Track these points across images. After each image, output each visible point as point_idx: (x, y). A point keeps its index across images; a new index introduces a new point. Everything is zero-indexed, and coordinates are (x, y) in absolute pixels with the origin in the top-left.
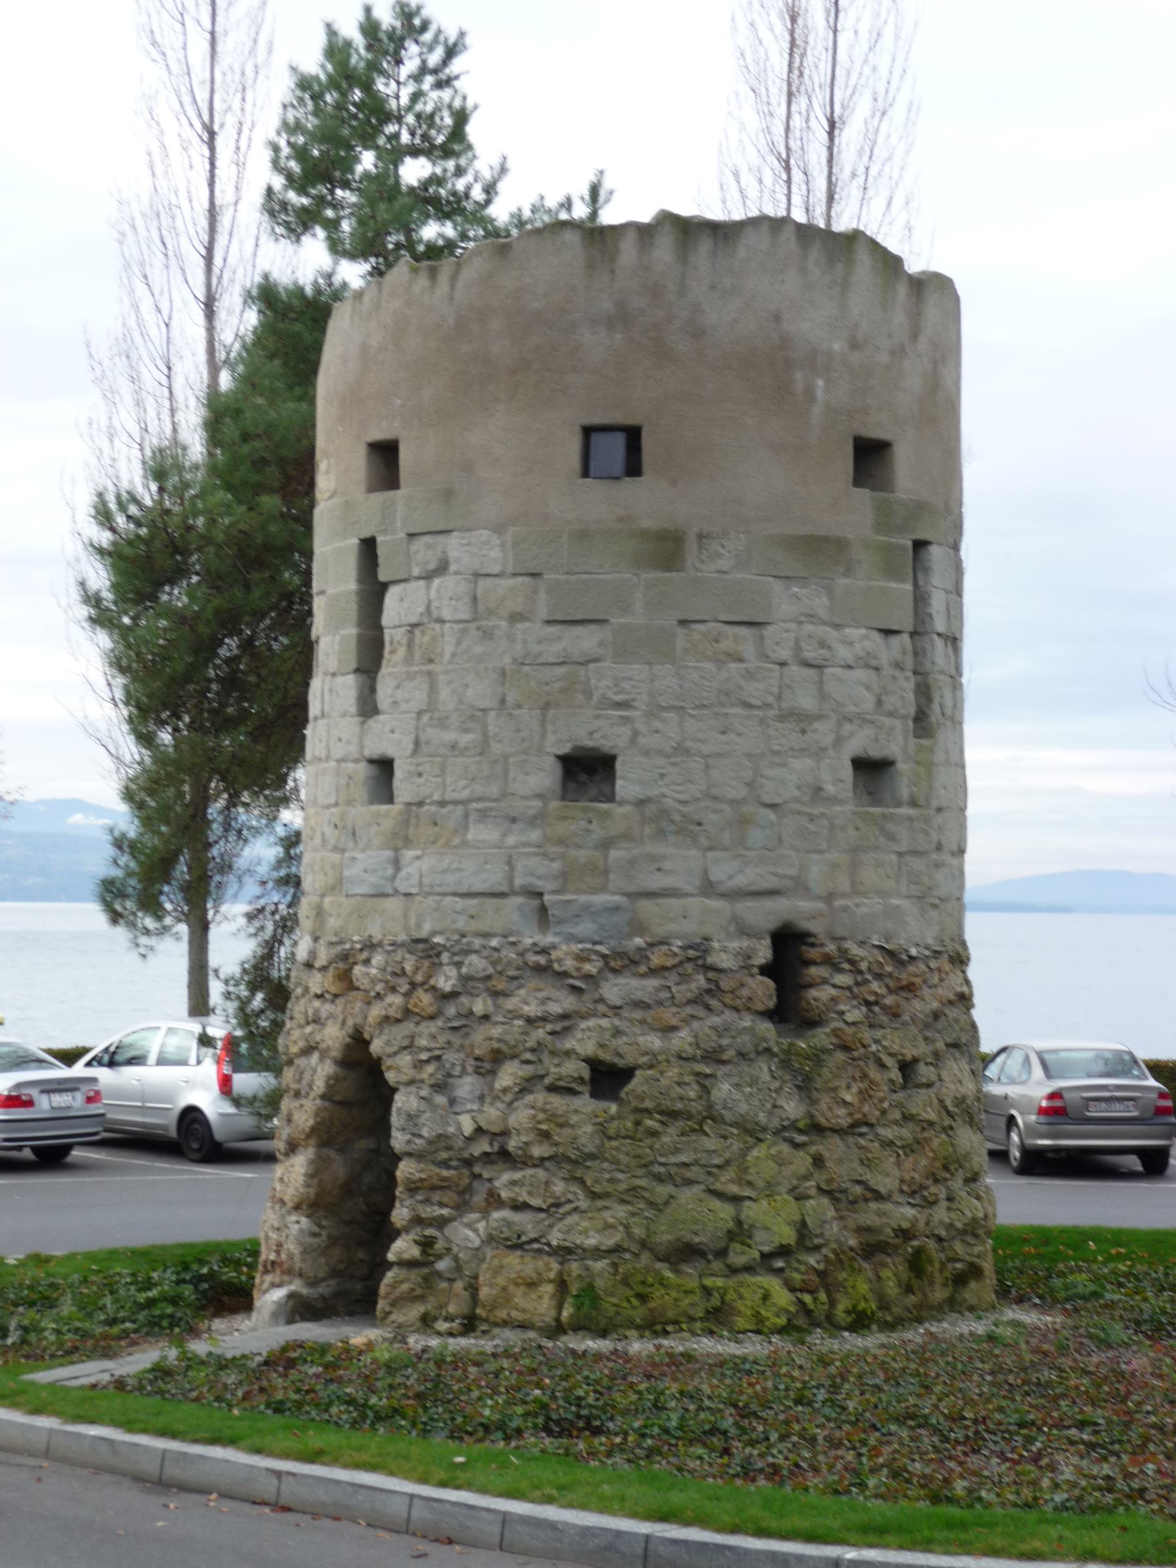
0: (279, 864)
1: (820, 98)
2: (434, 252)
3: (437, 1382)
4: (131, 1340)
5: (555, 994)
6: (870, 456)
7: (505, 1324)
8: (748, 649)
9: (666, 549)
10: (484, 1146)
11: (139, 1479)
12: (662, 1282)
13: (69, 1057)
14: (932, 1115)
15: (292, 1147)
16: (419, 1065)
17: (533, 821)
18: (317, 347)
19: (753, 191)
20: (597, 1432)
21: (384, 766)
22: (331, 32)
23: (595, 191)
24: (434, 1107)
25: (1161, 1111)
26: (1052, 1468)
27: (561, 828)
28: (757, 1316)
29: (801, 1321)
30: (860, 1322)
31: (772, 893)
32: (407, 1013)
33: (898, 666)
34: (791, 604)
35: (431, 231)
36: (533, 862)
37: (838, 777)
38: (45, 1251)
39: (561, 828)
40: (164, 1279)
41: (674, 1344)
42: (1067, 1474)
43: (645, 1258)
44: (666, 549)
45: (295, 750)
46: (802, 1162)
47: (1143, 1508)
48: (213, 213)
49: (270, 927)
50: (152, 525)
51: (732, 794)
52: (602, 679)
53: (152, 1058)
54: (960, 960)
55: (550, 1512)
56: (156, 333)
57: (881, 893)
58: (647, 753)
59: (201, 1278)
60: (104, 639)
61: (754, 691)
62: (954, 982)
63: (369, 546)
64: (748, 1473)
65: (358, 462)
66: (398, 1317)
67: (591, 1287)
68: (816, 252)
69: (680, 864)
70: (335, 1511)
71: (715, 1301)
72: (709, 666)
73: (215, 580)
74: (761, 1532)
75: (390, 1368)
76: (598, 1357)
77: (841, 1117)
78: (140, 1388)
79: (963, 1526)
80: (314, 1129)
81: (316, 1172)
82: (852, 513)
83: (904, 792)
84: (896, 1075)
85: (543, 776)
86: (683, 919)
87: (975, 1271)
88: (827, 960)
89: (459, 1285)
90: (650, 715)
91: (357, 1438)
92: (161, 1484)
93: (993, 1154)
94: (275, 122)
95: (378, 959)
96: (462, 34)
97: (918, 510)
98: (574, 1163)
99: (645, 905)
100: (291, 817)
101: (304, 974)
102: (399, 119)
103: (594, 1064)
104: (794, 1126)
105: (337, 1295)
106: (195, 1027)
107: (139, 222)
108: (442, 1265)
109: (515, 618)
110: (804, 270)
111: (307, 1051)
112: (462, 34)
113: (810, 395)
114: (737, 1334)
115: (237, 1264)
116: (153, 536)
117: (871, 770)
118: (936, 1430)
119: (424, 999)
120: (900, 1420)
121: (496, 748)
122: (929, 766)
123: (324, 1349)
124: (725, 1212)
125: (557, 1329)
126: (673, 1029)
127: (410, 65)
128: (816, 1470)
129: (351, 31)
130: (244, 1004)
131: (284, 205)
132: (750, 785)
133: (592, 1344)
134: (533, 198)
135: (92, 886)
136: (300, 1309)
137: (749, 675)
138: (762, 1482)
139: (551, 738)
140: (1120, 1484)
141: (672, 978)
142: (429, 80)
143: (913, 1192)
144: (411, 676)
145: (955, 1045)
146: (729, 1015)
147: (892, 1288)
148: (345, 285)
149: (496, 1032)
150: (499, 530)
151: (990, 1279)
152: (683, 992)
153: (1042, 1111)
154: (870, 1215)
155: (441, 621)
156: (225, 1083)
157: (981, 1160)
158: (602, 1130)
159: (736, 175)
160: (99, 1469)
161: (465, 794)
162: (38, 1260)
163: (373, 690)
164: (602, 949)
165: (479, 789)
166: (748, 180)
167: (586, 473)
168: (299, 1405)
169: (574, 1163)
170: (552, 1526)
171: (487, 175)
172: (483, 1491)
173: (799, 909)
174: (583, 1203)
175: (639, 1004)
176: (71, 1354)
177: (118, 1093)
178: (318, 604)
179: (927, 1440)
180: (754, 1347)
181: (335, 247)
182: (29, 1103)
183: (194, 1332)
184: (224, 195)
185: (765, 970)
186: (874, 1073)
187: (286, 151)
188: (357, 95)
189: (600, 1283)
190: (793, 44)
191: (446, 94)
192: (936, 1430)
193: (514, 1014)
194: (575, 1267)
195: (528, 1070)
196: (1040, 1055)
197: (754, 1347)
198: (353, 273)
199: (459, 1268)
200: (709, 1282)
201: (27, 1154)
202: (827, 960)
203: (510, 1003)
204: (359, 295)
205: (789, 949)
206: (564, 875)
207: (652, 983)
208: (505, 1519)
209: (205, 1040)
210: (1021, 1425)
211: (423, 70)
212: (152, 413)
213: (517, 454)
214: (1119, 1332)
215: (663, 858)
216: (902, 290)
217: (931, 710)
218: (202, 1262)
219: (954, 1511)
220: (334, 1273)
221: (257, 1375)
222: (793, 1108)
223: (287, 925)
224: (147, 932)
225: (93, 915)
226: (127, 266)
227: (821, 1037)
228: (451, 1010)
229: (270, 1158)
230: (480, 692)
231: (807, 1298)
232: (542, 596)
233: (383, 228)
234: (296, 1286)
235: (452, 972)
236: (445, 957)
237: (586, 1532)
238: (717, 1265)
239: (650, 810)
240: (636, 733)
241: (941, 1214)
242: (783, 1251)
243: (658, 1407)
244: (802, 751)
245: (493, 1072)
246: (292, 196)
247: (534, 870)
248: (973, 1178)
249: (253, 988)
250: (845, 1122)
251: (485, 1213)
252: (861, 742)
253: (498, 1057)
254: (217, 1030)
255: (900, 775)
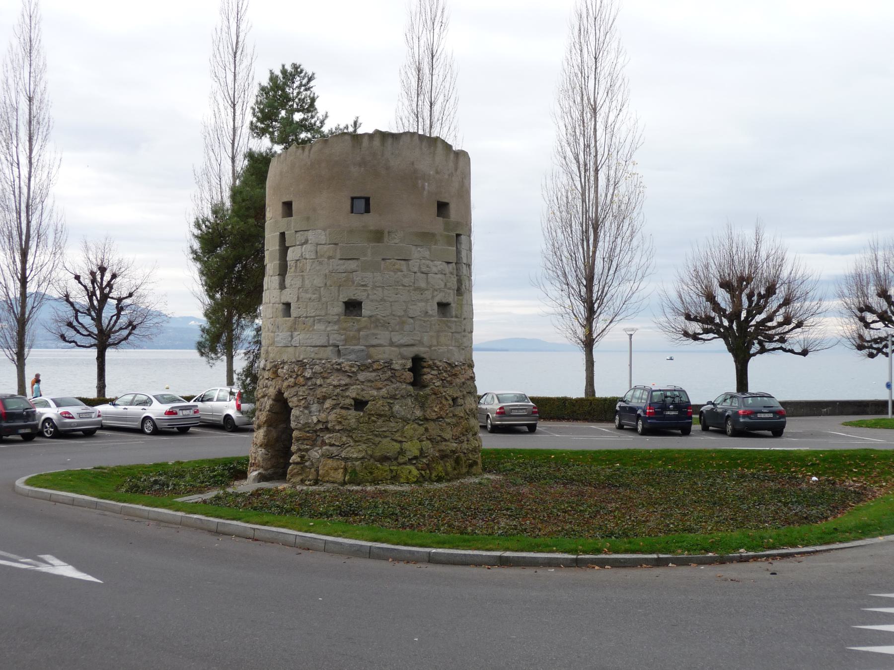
0: (255, 337)
1: (427, 96)
2: (304, 142)
3: (306, 500)
4: (209, 489)
5: (344, 378)
6: (442, 208)
7: (327, 482)
8: (404, 268)
9: (378, 236)
10: (320, 426)
11: (210, 531)
12: (377, 468)
13: (188, 399)
14: (462, 415)
15: (259, 427)
16: (299, 401)
17: (335, 323)
18: (267, 172)
19: (406, 124)
20: (356, 515)
21: (288, 305)
22: (272, 73)
23: (355, 123)
24: (304, 414)
25: (534, 413)
26: (498, 523)
27: (345, 325)
28: (407, 478)
29: (421, 479)
30: (439, 479)
31: (412, 345)
32: (295, 384)
33: (451, 273)
34: (418, 254)
35: (303, 135)
36: (335, 336)
37: (433, 309)
38: (181, 460)
39: (345, 325)
40: (219, 469)
41: (381, 487)
42: (503, 524)
43: (372, 460)
44: (378, 236)
45: (259, 301)
46: (421, 430)
47: (525, 534)
48: (234, 130)
49: (252, 357)
50: (213, 228)
51: (399, 314)
52: (357, 278)
53: (215, 399)
54: (471, 366)
55: (340, 540)
56: (216, 168)
57: (446, 345)
58: (372, 301)
59: (231, 468)
60: (199, 265)
61: (406, 281)
62: (469, 373)
63: (283, 235)
64: (404, 527)
65: (279, 208)
66: (293, 480)
67: (355, 470)
68: (424, 143)
69: (383, 336)
70: (272, 541)
71: (394, 474)
72: (392, 273)
73: (234, 246)
74: (406, 545)
75: (291, 496)
76: (357, 492)
77: (434, 416)
78: (211, 503)
79: (469, 541)
80: (266, 421)
81: (266, 435)
82: (437, 225)
83: (454, 313)
84: (451, 402)
85: (339, 308)
86: (383, 354)
87: (475, 463)
88: (430, 367)
89: (313, 470)
90: (373, 289)
91: (279, 518)
92: (217, 532)
93: (481, 426)
94: (254, 101)
95: (286, 367)
96: (313, 74)
97: (458, 224)
98: (349, 431)
99: (372, 349)
100: (258, 322)
101: (263, 372)
102: (293, 100)
103: (355, 399)
104: (419, 419)
105: (274, 473)
106: (229, 389)
107: (211, 132)
108: (307, 464)
109: (329, 258)
110: (421, 149)
111: (264, 396)
112: (313, 74)
113: (424, 189)
114: (401, 484)
115: (242, 464)
116: (214, 232)
117: (443, 306)
118: (462, 512)
119: (301, 380)
120: (451, 509)
121: (324, 299)
122: (461, 305)
123: (270, 490)
124: (397, 446)
125: (344, 483)
126: (381, 388)
127: (297, 84)
128: (425, 525)
129: (278, 72)
130: (244, 382)
131: (256, 127)
132: (405, 311)
133: (355, 488)
134: (336, 125)
135: (194, 344)
136: (262, 478)
137: (405, 276)
138: (408, 529)
139: (341, 296)
140: (519, 527)
141: (380, 373)
142: (303, 88)
143: (456, 438)
144: (296, 277)
145: (469, 393)
146: (398, 384)
147: (449, 469)
148: (275, 152)
149: (324, 390)
150: (324, 230)
151: (480, 465)
152: (383, 377)
153: (497, 413)
154: (443, 446)
155: (306, 259)
156: (239, 407)
157: (477, 428)
158: (358, 420)
159: (401, 119)
160: (197, 528)
161: (313, 314)
162: (179, 463)
163: (284, 281)
164: (358, 363)
165: (318, 313)
166: (405, 121)
167: (352, 212)
168: (262, 508)
169: (349, 431)
170: (341, 544)
171: (321, 118)
172: (319, 533)
173: (421, 350)
174: (352, 444)
175: (369, 381)
176: (189, 492)
177: (204, 410)
178: (266, 253)
179: (460, 515)
180: (406, 488)
181: (273, 140)
182: (176, 414)
183: (228, 485)
184: (238, 123)
185: (410, 370)
186: (444, 402)
187: (257, 110)
188: (280, 92)
189: (357, 469)
190: (419, 78)
191: (308, 93)
192: (462, 512)
193: (330, 384)
194: (349, 464)
195: (334, 402)
196: (497, 395)
197: (406, 488)
198: (278, 149)
199: (313, 464)
200: (392, 468)
201: (175, 429)
202: (430, 367)
203: (328, 381)
204: (280, 155)
205: (418, 363)
206: (346, 340)
207: (374, 374)
208: (326, 542)
209: (231, 393)
210: (489, 510)
211: (301, 85)
212: (214, 193)
213: (330, 206)
214: (519, 481)
215: (377, 334)
216: (452, 156)
217: (462, 287)
218: (231, 463)
219: (467, 537)
220: (273, 467)
221: (249, 498)
222: (418, 413)
223: (257, 356)
224: (212, 359)
225: (195, 354)
226: (207, 146)
227: (427, 391)
228: (310, 383)
229: (252, 431)
230: (318, 281)
231: (423, 472)
232: (338, 251)
233: (288, 135)
234: (261, 470)
235: (310, 371)
236: (308, 366)
237: (351, 545)
238: (395, 463)
239: (373, 319)
240: (368, 295)
241: (465, 445)
242: (416, 458)
243: (376, 507)
244: (422, 300)
245: (323, 403)
246: (259, 124)
247: (336, 338)
248: (475, 434)
249: (247, 377)
250: (435, 417)
251: (321, 447)
252: (440, 297)
253: (325, 398)
254: (236, 390)
255: (453, 309)
